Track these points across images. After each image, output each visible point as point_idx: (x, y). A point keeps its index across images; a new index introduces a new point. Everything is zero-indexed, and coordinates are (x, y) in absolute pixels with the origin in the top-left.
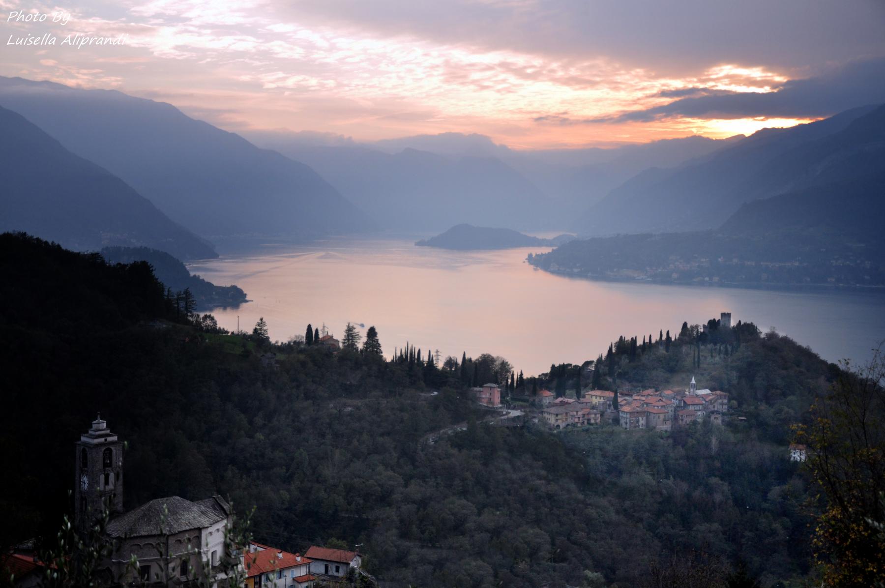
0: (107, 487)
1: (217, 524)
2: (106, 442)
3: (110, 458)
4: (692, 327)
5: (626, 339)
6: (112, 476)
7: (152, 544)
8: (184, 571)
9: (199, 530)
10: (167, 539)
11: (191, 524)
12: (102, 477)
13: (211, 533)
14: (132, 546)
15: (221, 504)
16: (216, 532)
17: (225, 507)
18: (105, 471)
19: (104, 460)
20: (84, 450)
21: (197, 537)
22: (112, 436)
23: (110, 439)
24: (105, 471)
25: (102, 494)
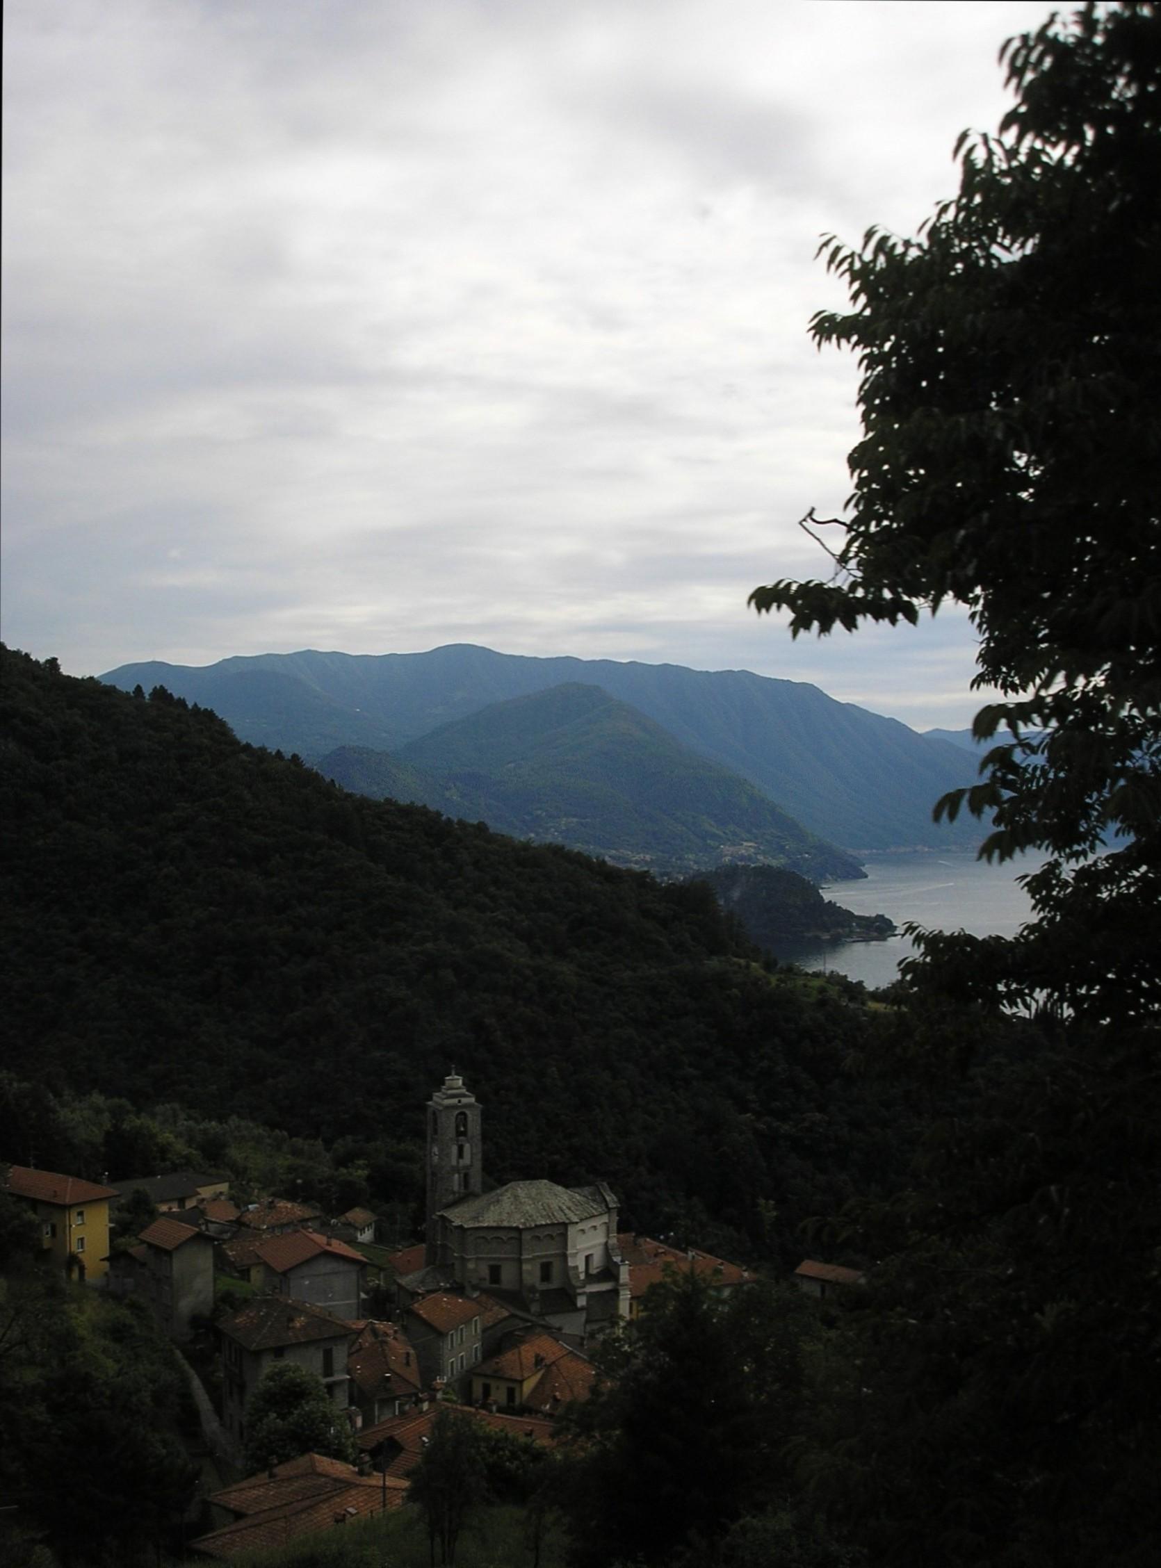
0: (461, 1161)
1: (593, 1219)
2: (459, 1104)
3: (465, 1126)
4: (1042, 903)
5: (269, 751)
6: (467, 1147)
7: (501, 1239)
8: (546, 1276)
9: (565, 1225)
10: (521, 1234)
11: (555, 1217)
12: (455, 1149)
13: (583, 1231)
14: (479, 1238)
15: (604, 1194)
16: (592, 1230)
17: (608, 1198)
18: (457, 1141)
19: (457, 1127)
20: (434, 1113)
21: (561, 1234)
22: (469, 1097)
23: (464, 1100)
24: (457, 1141)
25: (456, 1169)
